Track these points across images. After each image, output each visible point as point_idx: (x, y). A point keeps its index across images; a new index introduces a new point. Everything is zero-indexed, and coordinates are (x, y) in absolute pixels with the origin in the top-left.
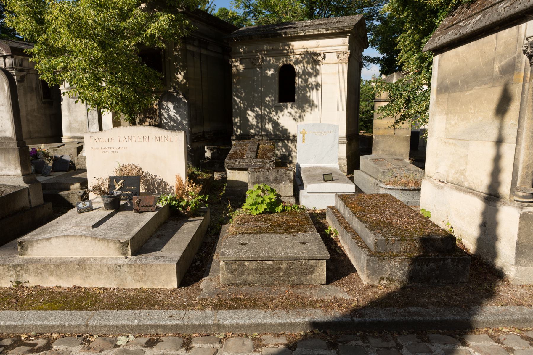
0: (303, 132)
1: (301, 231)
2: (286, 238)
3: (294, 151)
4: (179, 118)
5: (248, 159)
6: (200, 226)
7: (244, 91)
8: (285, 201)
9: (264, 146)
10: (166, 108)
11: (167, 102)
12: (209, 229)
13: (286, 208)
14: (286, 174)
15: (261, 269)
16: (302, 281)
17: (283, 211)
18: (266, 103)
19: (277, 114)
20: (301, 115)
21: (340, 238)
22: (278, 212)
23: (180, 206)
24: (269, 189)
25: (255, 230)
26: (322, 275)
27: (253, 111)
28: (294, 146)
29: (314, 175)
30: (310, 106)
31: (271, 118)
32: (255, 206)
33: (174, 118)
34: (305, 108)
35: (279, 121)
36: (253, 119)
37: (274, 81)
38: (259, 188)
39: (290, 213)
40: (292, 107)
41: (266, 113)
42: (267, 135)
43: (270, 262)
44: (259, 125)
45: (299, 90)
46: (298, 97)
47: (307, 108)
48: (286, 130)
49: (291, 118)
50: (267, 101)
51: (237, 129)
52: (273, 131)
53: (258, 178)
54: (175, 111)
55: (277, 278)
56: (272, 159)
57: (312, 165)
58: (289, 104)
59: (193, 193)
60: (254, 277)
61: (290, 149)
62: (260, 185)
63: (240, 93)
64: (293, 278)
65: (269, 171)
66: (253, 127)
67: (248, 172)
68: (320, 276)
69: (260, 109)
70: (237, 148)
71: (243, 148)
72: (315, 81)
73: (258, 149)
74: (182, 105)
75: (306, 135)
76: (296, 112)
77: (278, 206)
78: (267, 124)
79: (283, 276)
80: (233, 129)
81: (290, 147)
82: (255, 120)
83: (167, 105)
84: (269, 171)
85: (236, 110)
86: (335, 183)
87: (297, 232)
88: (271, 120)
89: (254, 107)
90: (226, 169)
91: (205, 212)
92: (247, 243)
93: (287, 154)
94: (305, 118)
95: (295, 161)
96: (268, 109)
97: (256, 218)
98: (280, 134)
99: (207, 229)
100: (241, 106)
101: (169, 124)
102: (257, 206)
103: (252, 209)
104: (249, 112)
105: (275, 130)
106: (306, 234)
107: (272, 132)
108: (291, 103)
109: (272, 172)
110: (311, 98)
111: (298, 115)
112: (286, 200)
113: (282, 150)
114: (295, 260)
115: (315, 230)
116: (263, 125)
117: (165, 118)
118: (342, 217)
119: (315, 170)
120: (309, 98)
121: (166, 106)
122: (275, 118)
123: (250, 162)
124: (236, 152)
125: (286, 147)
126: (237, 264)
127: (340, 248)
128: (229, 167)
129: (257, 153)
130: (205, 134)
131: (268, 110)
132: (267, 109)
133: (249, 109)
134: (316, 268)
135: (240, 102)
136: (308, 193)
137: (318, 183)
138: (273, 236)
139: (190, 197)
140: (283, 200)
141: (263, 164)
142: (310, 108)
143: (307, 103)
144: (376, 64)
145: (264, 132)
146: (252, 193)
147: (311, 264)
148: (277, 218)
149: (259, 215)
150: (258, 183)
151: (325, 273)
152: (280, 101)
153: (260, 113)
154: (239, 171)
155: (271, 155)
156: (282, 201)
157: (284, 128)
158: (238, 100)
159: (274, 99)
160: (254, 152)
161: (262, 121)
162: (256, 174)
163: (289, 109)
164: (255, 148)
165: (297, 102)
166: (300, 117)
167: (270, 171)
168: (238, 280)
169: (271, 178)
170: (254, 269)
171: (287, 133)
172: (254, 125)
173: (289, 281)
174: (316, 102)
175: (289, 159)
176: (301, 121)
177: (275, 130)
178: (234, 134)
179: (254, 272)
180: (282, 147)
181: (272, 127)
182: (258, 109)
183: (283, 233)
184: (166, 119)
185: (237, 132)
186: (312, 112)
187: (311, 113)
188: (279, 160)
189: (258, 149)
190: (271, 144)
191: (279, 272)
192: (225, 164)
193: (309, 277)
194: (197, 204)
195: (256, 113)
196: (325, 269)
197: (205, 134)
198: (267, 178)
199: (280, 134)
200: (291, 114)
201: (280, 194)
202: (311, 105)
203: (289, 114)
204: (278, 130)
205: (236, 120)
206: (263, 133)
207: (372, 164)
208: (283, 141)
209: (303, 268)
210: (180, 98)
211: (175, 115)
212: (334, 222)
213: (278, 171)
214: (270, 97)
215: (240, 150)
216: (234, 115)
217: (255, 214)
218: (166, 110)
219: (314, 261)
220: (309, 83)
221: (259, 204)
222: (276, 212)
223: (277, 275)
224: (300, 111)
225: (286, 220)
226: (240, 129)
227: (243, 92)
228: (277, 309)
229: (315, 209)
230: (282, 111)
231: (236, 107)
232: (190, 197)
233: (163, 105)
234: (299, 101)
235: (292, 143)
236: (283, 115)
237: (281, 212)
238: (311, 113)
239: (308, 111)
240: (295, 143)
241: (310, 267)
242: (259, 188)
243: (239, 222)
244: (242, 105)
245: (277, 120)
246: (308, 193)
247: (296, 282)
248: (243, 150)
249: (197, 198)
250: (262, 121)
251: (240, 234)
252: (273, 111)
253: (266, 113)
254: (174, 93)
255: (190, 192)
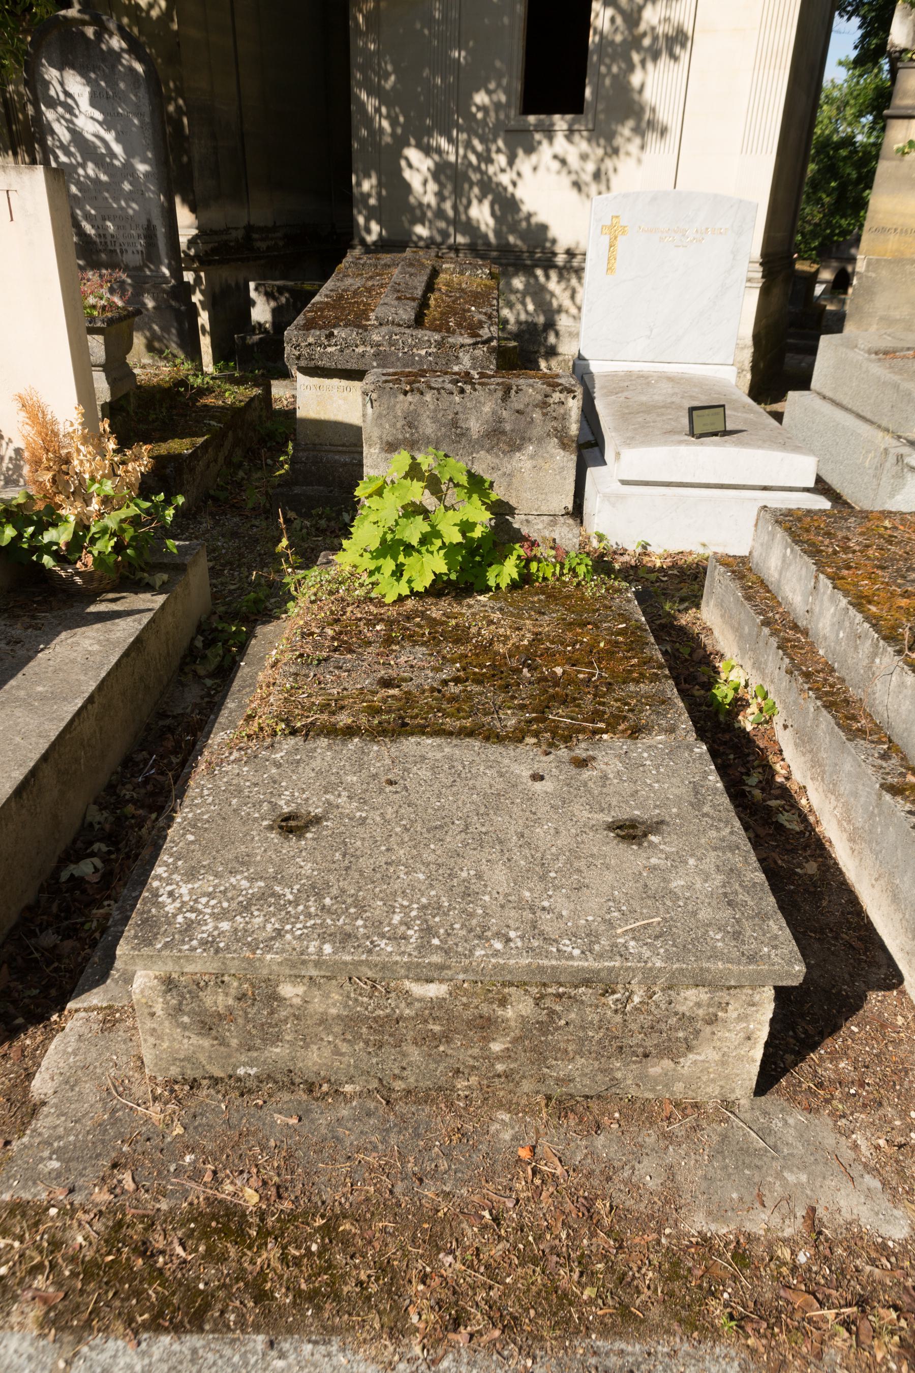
0: (612, 226)
1: (611, 728)
2: (537, 777)
3: (567, 312)
4: (117, 149)
5: (384, 330)
6: (138, 644)
7: (394, 63)
8: (534, 536)
9: (456, 278)
10: (62, 97)
11: (61, 69)
12: (199, 643)
13: (534, 566)
14: (544, 404)
15: (375, 1020)
16: (614, 1080)
17: (525, 580)
18: (474, 115)
19: (511, 162)
20: (603, 168)
21: (785, 739)
22: (498, 587)
23: (46, 549)
24: (463, 479)
25: (374, 711)
26: (740, 1058)
27: (427, 150)
28: (568, 293)
29: (648, 409)
30: (639, 131)
31: (490, 178)
32: (395, 558)
33: (96, 147)
34: (619, 141)
35: (519, 193)
36: (425, 183)
37: (506, 20)
38: (414, 471)
39: (553, 596)
40: (570, 134)
41: (473, 159)
42: (472, 248)
43: (435, 990)
44: (448, 206)
45: (600, 61)
46: (595, 93)
47: (629, 140)
48: (544, 228)
49: (566, 181)
50: (479, 108)
51: (367, 220)
52: (497, 233)
53: (411, 422)
54: (99, 116)
55: (471, 1062)
56: (485, 333)
57: (636, 367)
58: (560, 122)
59: (108, 487)
60: (337, 1052)
61: (555, 304)
62: (420, 458)
63: (378, 74)
64: (565, 1068)
65: (462, 391)
66: (424, 214)
67: (365, 393)
68: (723, 1063)
69: (450, 140)
70: (348, 281)
71: (370, 283)
72: (667, 20)
73: (430, 287)
74: (122, 85)
75: (621, 241)
76: (584, 157)
77: (501, 559)
78: (475, 202)
79: (507, 1055)
80: (352, 221)
81: (552, 295)
82: (432, 187)
83: (62, 84)
84: (462, 391)
85: (362, 141)
86: (716, 444)
87: (595, 732)
88: (489, 188)
89: (430, 135)
90: (294, 371)
91: (177, 568)
92: (317, 820)
93: (541, 319)
94: (615, 181)
95: (567, 349)
96: (481, 142)
97: (390, 623)
98: (519, 243)
99: (193, 639)
100: (381, 129)
101: (81, 171)
102: (401, 558)
103: (378, 569)
104: (413, 154)
105: (504, 229)
106: (641, 748)
107: (491, 236)
108: (569, 117)
109: (481, 393)
110: (649, 96)
111: (590, 167)
112: (535, 529)
113: (524, 304)
114: (587, 983)
115: (685, 724)
116: (461, 209)
117: (63, 147)
118: (795, 627)
119: (648, 384)
120: (636, 96)
121: (59, 88)
122: (505, 179)
123: (392, 343)
124: (342, 296)
125: (539, 293)
126: (233, 991)
127: (785, 793)
128: (303, 363)
129: (424, 304)
130: (255, 236)
131: (479, 147)
132: (476, 143)
133: (413, 141)
134: (708, 1029)
135: (378, 110)
136: (624, 482)
137: (665, 443)
138: (468, 756)
139: (95, 506)
140: (525, 531)
141: (445, 350)
142: (637, 141)
143: (626, 117)
144: (849, 19)
145: (464, 234)
146: (379, 492)
147: (681, 1009)
148: (490, 622)
149: (410, 603)
150: (412, 445)
151: (758, 1053)
152: (527, 109)
153: (452, 158)
154: (344, 383)
155: (483, 318)
156: (518, 537)
157: (534, 220)
158: (371, 103)
159: (503, 98)
160: (413, 299)
161: (458, 193)
162: (404, 403)
163: (560, 144)
164: (419, 284)
165: (590, 116)
166: (597, 176)
167: (468, 388)
168: (245, 1064)
169: (475, 426)
170: (339, 1016)
171: (546, 239)
172: (429, 206)
173: (542, 1080)
174: (666, 114)
175: (546, 339)
176: (600, 193)
177: (504, 229)
178: (356, 241)
179: (337, 1029)
180: (525, 294)
181: (493, 214)
182: (443, 143)
183: (518, 737)
184: (68, 153)
185: (368, 231)
186: (647, 156)
187: (639, 161)
188: (513, 344)
189: (430, 287)
190: (483, 273)
191: (487, 1040)
192: (288, 348)
193: (657, 1068)
194: (127, 538)
195: (436, 157)
196: (763, 1034)
197: (255, 236)
198: (455, 424)
199: (519, 243)
200: (563, 162)
201: (513, 502)
202: (644, 124)
203: (556, 165)
204: (514, 228)
205: (366, 186)
206: (461, 239)
207: (877, 370)
208: (528, 271)
209: (634, 1027)
210: (111, 50)
211: (102, 132)
212: (749, 645)
213: (507, 390)
214: (489, 92)
215: (355, 293)
216: (357, 164)
217: (389, 600)
218: (60, 110)
219: (703, 995)
220: (643, 27)
221: (409, 549)
222: (488, 589)
223: (476, 1051)
224: (600, 152)
225: (537, 638)
226: (379, 222)
227: (390, 68)
228: (461, 1338)
229: (644, 547)
230: (530, 149)
231: (364, 132)
232: (95, 506)
233: (47, 84)
234: (600, 107)
235: (561, 277)
236: (535, 169)
237: (514, 586)
238: (639, 161)
239: (628, 154)
240: (574, 282)
241: (673, 1021)
242: (414, 471)
243: (308, 649)
244: (385, 124)
245: (510, 189)
246: (624, 482)
247: (581, 1086)
248: (369, 290)
249: (124, 513)
250: (458, 193)
251: (294, 732)
252: (499, 151)
253: (473, 159)
254: (84, 23)
255: (93, 479)
